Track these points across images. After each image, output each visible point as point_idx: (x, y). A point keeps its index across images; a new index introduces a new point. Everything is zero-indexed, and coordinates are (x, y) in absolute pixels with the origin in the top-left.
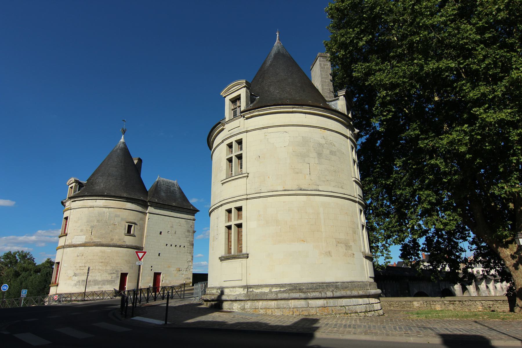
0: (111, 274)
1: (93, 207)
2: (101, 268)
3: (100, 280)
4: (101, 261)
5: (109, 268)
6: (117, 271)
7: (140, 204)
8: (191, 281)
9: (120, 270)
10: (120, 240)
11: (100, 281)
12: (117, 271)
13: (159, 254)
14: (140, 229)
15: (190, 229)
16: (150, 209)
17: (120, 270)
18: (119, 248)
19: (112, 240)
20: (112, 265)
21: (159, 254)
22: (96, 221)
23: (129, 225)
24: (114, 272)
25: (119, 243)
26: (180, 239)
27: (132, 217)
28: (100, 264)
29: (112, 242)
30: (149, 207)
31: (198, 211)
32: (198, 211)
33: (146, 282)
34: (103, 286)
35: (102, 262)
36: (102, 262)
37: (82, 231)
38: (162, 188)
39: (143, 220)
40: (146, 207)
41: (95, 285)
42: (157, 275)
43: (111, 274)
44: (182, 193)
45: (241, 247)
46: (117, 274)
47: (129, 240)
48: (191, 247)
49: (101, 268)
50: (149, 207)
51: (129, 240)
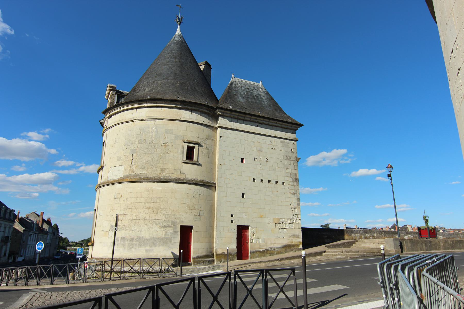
0: (165, 227)
1: (132, 121)
2: (147, 217)
3: (149, 238)
4: (147, 205)
5: (160, 217)
6: (173, 223)
8: (301, 240)
9: (178, 221)
10: (175, 170)
12: (173, 223)
13: (243, 195)
14: (208, 153)
15: (290, 155)
16: (222, 121)
17: (178, 221)
18: (175, 184)
19: (163, 170)
20: (165, 212)
21: (243, 195)
22: (137, 142)
24: (170, 223)
25: (174, 176)
26: (275, 170)
27: (194, 133)
28: (147, 211)
29: (164, 175)
30: (220, 118)
31: (301, 125)
32: (301, 125)
33: (226, 242)
34: (154, 248)
35: (149, 208)
36: (149, 208)
37: (119, 159)
38: (239, 91)
40: (215, 118)
41: (140, 246)
42: (242, 231)
43: (165, 227)
44: (272, 99)
46: (175, 228)
47: (190, 172)
48: (295, 184)
49: (147, 217)
50: (220, 118)
51: (190, 172)
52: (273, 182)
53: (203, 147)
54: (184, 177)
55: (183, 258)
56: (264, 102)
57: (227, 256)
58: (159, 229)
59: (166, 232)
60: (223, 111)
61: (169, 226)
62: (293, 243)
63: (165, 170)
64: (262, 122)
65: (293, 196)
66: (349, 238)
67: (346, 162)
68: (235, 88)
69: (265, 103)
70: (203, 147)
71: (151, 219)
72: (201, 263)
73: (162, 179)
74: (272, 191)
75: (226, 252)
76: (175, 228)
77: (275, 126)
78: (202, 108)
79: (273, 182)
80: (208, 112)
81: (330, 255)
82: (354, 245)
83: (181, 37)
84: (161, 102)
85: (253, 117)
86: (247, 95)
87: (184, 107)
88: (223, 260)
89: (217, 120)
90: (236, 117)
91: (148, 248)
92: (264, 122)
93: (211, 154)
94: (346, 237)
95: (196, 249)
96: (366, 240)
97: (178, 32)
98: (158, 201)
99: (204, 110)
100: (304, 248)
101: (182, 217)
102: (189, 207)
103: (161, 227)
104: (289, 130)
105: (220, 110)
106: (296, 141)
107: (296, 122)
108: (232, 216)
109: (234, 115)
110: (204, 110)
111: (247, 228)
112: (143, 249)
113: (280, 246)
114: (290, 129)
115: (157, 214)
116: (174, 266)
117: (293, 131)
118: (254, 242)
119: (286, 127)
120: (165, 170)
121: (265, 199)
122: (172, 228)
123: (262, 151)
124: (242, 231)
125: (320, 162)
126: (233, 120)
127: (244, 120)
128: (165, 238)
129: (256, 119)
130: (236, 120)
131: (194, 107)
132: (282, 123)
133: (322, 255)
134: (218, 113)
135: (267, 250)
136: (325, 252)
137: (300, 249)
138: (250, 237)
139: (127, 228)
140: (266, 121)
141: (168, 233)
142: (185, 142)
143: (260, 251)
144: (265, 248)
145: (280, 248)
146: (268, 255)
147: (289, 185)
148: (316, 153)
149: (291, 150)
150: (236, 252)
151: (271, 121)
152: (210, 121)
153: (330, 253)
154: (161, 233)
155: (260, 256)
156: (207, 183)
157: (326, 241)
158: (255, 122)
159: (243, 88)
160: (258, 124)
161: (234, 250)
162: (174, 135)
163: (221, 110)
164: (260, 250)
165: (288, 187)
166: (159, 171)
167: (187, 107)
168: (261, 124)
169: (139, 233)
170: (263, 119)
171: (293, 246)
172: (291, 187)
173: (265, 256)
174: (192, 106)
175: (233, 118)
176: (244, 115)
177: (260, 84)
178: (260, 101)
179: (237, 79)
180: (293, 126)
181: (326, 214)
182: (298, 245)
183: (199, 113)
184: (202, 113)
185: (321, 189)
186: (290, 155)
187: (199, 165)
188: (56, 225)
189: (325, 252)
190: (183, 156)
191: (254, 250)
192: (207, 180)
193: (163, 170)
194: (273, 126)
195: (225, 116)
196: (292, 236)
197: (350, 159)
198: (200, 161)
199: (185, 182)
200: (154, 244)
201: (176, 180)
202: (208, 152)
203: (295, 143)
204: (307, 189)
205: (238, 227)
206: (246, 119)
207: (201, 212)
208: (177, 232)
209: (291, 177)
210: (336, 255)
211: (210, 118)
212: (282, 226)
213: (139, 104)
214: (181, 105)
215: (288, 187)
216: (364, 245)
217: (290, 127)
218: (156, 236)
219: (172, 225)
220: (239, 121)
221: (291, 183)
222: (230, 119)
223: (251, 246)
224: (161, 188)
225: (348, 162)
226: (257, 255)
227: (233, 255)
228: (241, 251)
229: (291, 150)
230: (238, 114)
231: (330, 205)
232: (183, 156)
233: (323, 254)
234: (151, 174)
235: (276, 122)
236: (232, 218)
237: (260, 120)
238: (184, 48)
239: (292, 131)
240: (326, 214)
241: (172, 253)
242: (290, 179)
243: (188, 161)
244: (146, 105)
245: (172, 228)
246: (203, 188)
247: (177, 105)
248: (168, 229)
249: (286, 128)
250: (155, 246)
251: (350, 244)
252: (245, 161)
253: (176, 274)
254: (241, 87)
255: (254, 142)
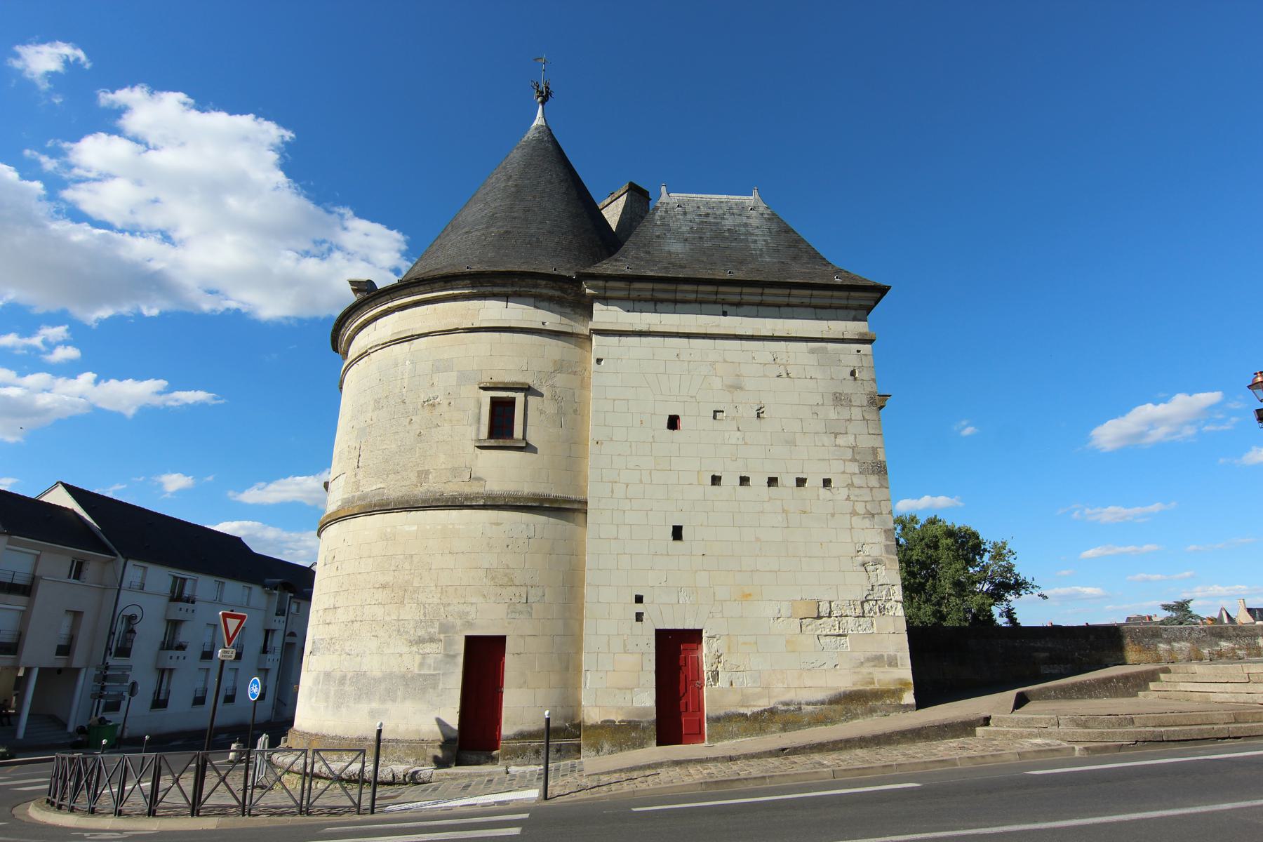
0: (421, 641)
2: (379, 611)
3: (378, 674)
4: (382, 579)
5: (410, 612)
6: (445, 628)
7: (550, 299)
8: (906, 673)
9: (458, 623)
10: (455, 472)
11: (378, 681)
12: (445, 628)
14: (561, 412)
15: (849, 387)
16: (605, 315)
17: (458, 623)
18: (454, 513)
19: (423, 475)
20: (422, 598)
23: (495, 402)
24: (434, 630)
25: (453, 488)
26: (792, 443)
27: (509, 360)
28: (380, 595)
29: (425, 487)
30: (597, 307)
32: (882, 291)
33: (619, 684)
34: (389, 705)
35: (384, 587)
36: (384, 587)
38: (674, 225)
39: (575, 371)
40: (584, 308)
41: (358, 698)
42: (675, 652)
43: (421, 641)
44: (787, 230)
45: (1056, 698)
46: (449, 644)
47: (502, 471)
48: (873, 480)
50: (597, 307)
51: (502, 471)
52: (788, 481)
53: (541, 395)
54: (481, 490)
55: (475, 737)
56: (755, 242)
57: (621, 733)
58: (405, 649)
59: (424, 656)
60: (601, 283)
61: (432, 640)
62: (876, 686)
63: (427, 472)
64: (737, 298)
65: (867, 523)
66: (1143, 657)
67: (1222, 428)
68: (662, 218)
69: (761, 244)
70: (541, 395)
71: (387, 618)
72: (530, 754)
73: (417, 501)
74: (784, 511)
75: (543, 725)
76: (449, 644)
77: (788, 305)
78: (536, 286)
79: (788, 481)
80: (557, 293)
81: (1005, 734)
82: (1152, 685)
83: (548, 130)
84: (422, 288)
85: (702, 288)
86: (700, 231)
87: (483, 290)
88: (606, 747)
89: (590, 315)
90: (648, 295)
91: (375, 705)
92: (746, 298)
93: (571, 414)
94: (1131, 654)
95: (520, 708)
96: (1196, 667)
97: (539, 121)
98: (407, 566)
99: (545, 291)
100: (924, 699)
101: (472, 609)
102: (493, 579)
103: (412, 643)
104: (840, 312)
105: (590, 283)
106: (870, 341)
107: (860, 283)
108: (639, 599)
109: (640, 290)
110: (545, 291)
111: (694, 637)
112: (364, 707)
113: (820, 696)
114: (846, 308)
115: (402, 602)
116: (440, 763)
117: (861, 312)
118: (725, 683)
119: (827, 302)
120: (427, 472)
121: (758, 539)
122: (441, 645)
123: (741, 388)
124: (675, 652)
125: (1141, 435)
126: (637, 305)
127: (676, 302)
128: (420, 675)
129: (717, 293)
130: (651, 305)
131: (512, 285)
132: (808, 292)
133: (973, 733)
134: (588, 291)
135: (772, 712)
136: (986, 721)
137: (906, 707)
138: (706, 668)
139: (337, 647)
140: (751, 294)
141: (430, 661)
142: (485, 389)
143: (744, 715)
144: (763, 704)
145: (823, 703)
146: (774, 727)
147: (850, 486)
148: (1121, 410)
149: (853, 373)
150: (653, 716)
151: (767, 291)
152: (565, 321)
153: (1013, 729)
154: (407, 660)
155: (746, 733)
156: (556, 500)
157: (1045, 670)
158: (715, 302)
159: (689, 217)
160: (726, 308)
161: (645, 710)
162: (455, 374)
163: (595, 283)
164: (742, 710)
165: (844, 493)
166: (413, 477)
167: (489, 289)
168: (739, 304)
169: (359, 659)
170: (738, 290)
171: (877, 695)
172: (857, 491)
173: (762, 731)
174: (504, 286)
175: (640, 300)
176: (673, 287)
177: (751, 199)
178: (741, 241)
179: (676, 197)
180: (860, 297)
181: (1187, 574)
182: (896, 693)
183: (532, 300)
184: (538, 300)
185: (1156, 507)
186: (849, 387)
187: (527, 448)
188: (1129, 619)
189: (986, 721)
190: (478, 429)
191: (722, 713)
192: (554, 491)
193: (423, 475)
194: (779, 306)
195: (612, 298)
196: (868, 660)
197: (1234, 419)
198: (532, 438)
199: (481, 503)
200: (390, 695)
201: (454, 498)
202: (560, 408)
203: (866, 348)
204: (1111, 509)
205: (661, 634)
206: (679, 296)
207: (532, 591)
208: (454, 656)
209: (854, 460)
210: (1030, 735)
211: (568, 310)
212: (827, 625)
213: (372, 308)
214: (473, 287)
215: (844, 493)
216: (1190, 687)
217: (844, 302)
218: (396, 669)
219: (442, 636)
220: (659, 306)
221: (858, 481)
222: (629, 304)
223: (715, 697)
224: (415, 528)
225: (1227, 427)
226: (733, 727)
227: (644, 729)
228: (676, 714)
229: (853, 373)
230: (650, 286)
231: (1192, 547)
232: (478, 429)
233: (980, 730)
234: (395, 489)
235: (787, 291)
236: (639, 608)
237: (731, 293)
238: (552, 152)
239: (853, 313)
240: (1187, 574)
241: (439, 721)
242: (854, 468)
243: (493, 442)
244: (390, 305)
245: (441, 645)
246: (540, 519)
247: (463, 288)
248: (430, 648)
249: (830, 307)
250: (394, 700)
251: (1140, 682)
252: (682, 423)
253: (358, 806)
254: (685, 213)
255: (713, 364)
